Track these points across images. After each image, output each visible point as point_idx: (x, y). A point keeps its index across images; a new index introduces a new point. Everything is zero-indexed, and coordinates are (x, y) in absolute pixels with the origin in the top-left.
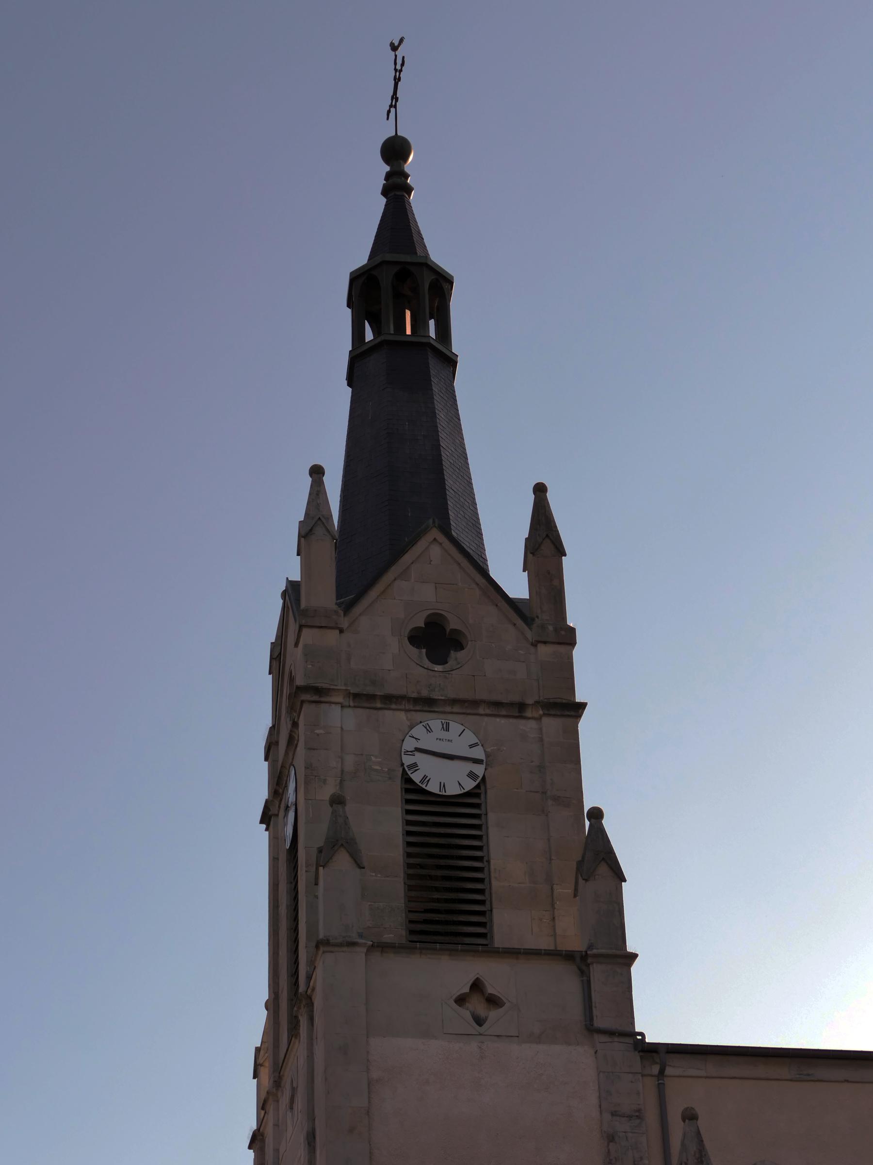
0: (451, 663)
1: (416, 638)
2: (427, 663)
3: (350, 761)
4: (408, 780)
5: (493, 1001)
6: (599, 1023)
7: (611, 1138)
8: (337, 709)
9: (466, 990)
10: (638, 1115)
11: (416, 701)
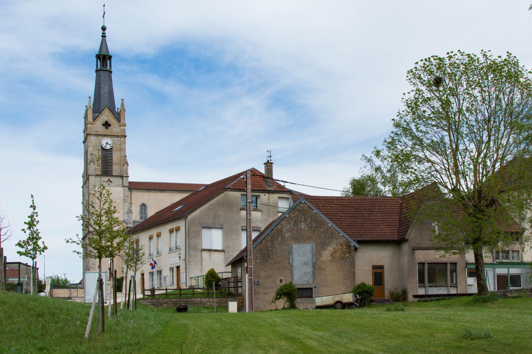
0: (109, 129)
1: (104, 125)
2: (105, 129)
3: (94, 144)
4: (102, 146)
5: (111, 182)
6: (124, 185)
7: (124, 199)
8: (92, 137)
9: (102, 31)
10: (128, 197)
11: (103, 135)
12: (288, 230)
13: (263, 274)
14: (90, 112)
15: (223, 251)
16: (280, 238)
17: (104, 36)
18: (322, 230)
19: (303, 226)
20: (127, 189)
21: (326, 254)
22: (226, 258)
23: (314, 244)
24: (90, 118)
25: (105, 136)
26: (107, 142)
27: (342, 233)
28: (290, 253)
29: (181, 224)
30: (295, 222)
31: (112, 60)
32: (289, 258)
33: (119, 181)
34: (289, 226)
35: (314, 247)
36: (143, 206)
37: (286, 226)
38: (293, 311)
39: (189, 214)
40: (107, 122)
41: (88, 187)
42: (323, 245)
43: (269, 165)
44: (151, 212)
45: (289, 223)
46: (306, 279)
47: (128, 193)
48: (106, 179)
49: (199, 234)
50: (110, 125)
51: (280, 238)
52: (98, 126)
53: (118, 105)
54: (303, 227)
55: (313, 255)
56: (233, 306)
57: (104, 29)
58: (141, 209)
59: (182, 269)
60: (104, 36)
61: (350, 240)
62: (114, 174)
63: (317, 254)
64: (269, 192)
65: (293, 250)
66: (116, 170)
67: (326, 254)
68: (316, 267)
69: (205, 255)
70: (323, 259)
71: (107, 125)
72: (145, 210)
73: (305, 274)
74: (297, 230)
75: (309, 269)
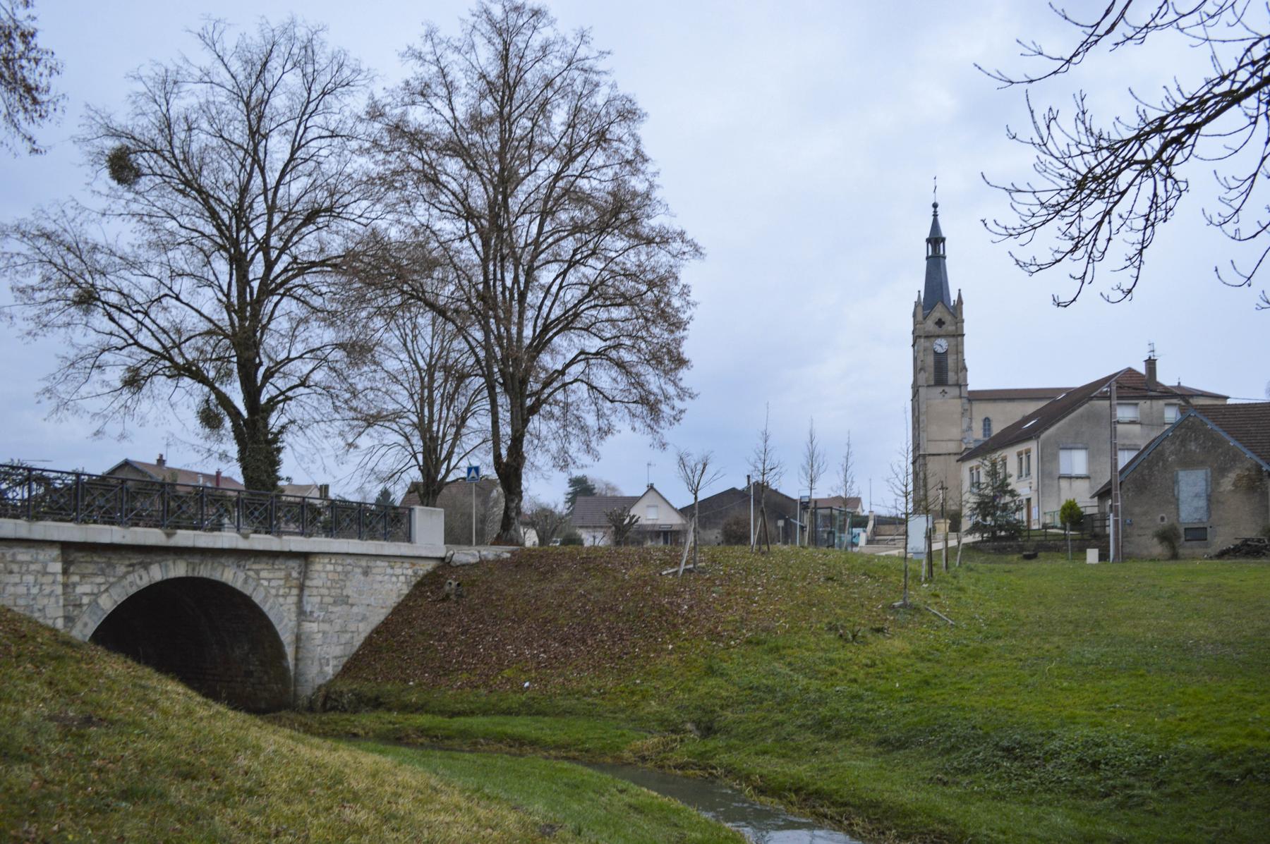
1: (936, 323)
12: (1172, 453)
13: (1137, 510)
14: (920, 310)
15: (1087, 477)
16: (1161, 464)
17: (935, 215)
18: (1220, 450)
19: (1192, 446)
20: (965, 401)
21: (1227, 483)
22: (1091, 487)
23: (1209, 470)
24: (920, 318)
25: (938, 336)
26: (941, 345)
27: (1249, 455)
28: (1175, 482)
29: (1033, 446)
30: (1182, 441)
31: (946, 242)
32: (1173, 490)
33: (955, 391)
34: (1173, 447)
35: (1209, 474)
36: (987, 421)
37: (1169, 448)
38: (1173, 566)
39: (1042, 432)
40: (940, 320)
41: (918, 401)
42: (1222, 471)
43: (1151, 363)
44: (996, 429)
45: (1173, 444)
46: (1197, 516)
47: (967, 406)
48: (940, 389)
49: (1055, 458)
50: (944, 323)
51: (1161, 464)
52: (930, 325)
53: (954, 297)
54: (1193, 448)
55: (1207, 485)
56: (1092, 555)
57: (935, 206)
58: (984, 425)
59: (1034, 503)
60: (935, 215)
61: (1261, 463)
62: (950, 382)
63: (1214, 482)
64: (1152, 398)
65: (1180, 478)
66: (951, 377)
67: (1227, 483)
68: (1212, 500)
69: (1064, 483)
70: (1222, 489)
71: (940, 323)
72: (989, 425)
73: (1197, 509)
74: (1185, 452)
75: (1202, 503)
